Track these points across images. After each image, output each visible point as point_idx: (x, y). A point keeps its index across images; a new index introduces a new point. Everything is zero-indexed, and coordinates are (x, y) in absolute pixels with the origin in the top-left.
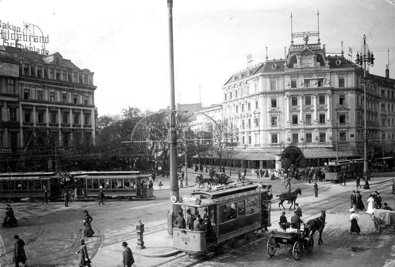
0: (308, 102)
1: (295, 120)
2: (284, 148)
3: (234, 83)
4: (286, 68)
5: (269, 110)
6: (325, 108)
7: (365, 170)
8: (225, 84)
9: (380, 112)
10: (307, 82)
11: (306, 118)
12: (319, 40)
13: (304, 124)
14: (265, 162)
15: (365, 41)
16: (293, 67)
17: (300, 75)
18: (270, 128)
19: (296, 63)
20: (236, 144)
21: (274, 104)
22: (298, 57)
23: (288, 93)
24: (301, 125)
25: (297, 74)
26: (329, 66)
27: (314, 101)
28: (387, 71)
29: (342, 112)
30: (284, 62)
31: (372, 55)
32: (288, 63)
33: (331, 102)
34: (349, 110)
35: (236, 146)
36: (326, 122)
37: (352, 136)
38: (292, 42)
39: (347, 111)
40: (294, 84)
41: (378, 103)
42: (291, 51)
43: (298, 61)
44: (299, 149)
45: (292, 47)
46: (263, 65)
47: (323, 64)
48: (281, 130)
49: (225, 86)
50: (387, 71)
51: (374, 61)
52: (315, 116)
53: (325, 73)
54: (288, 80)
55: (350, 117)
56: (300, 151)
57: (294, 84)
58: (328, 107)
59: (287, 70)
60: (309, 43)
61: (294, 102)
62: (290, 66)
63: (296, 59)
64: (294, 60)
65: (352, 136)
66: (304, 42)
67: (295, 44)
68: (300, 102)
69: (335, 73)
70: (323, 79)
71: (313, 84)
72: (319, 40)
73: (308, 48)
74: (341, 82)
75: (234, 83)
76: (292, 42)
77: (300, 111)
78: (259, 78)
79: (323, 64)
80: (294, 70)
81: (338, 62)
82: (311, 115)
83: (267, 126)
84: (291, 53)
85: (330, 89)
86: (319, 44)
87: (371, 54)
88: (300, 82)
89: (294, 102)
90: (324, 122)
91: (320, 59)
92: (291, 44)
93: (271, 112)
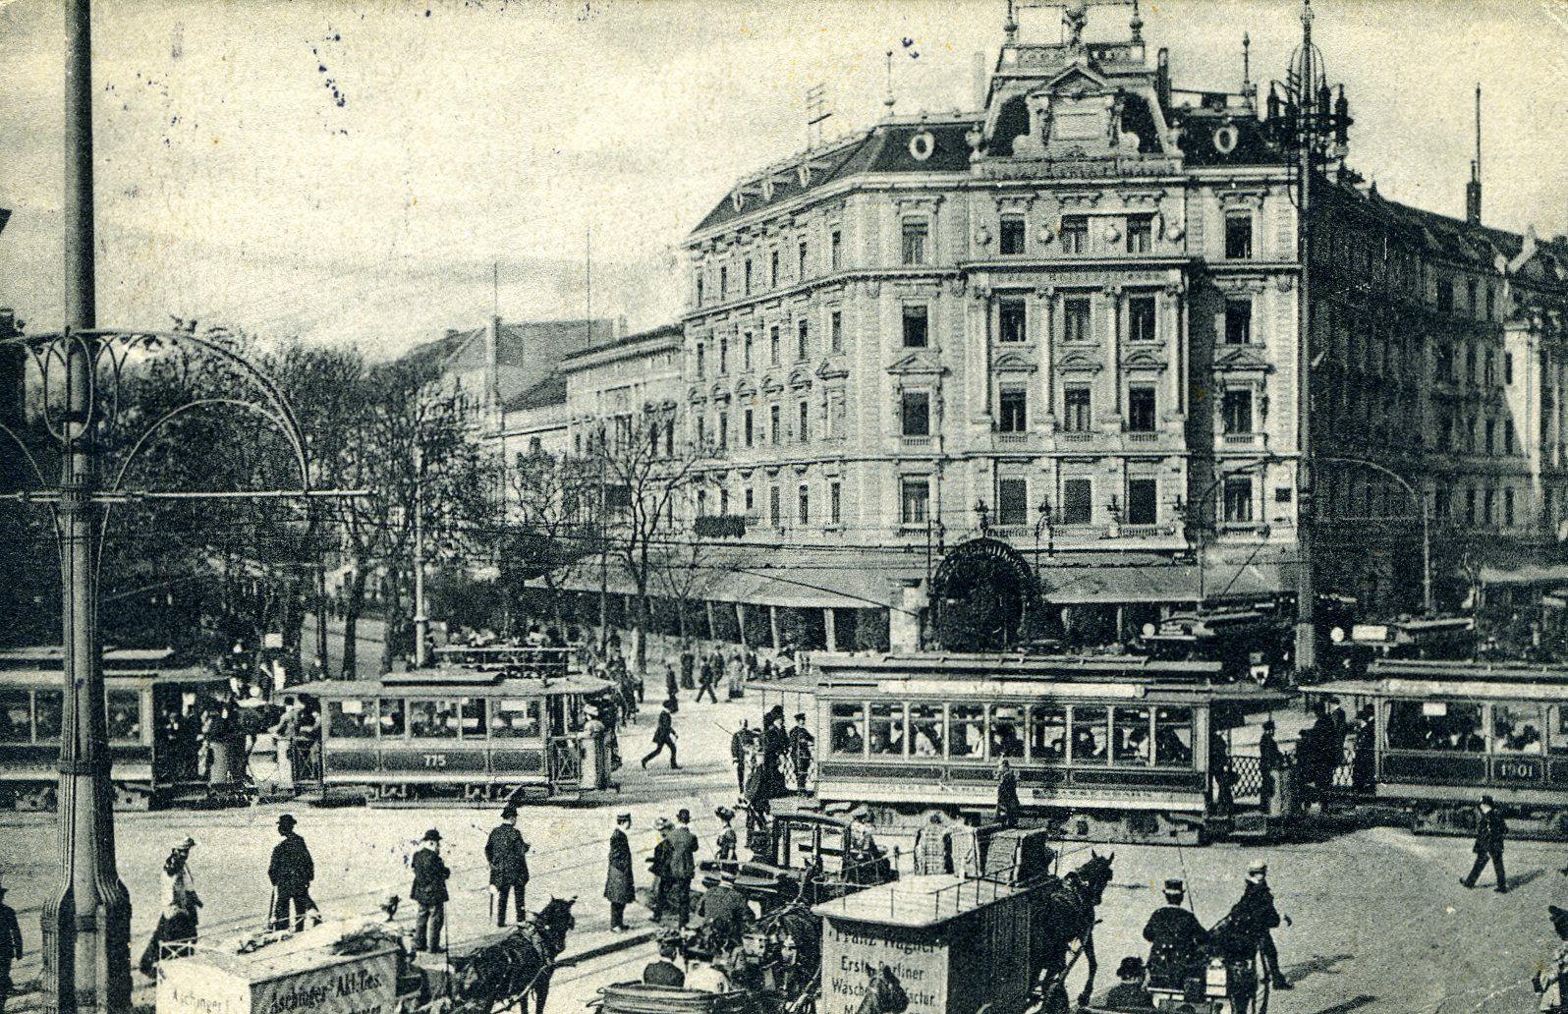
0: (1143, 322)
1: (1011, 412)
2: (941, 549)
3: (741, 222)
4: (976, 155)
5: (887, 357)
6: (1098, 358)
7: (170, 785)
8: (701, 227)
9: (1427, 384)
10: (1075, 226)
11: (1069, 402)
12: (1137, 26)
13: (1123, 430)
14: (845, 617)
15: (1307, 28)
16: (1010, 152)
17: (1045, 194)
18: (895, 446)
19: (1027, 132)
20: (738, 525)
21: (915, 329)
22: (1032, 105)
23: (983, 280)
24: (1040, 433)
25: (1031, 189)
26: (1180, 153)
27: (1106, 323)
28: (1474, 190)
29: (917, 385)
30: (968, 127)
31: (1342, 103)
32: (989, 131)
33: (1305, 321)
34: (1269, 370)
35: (741, 533)
36: (1028, 428)
37: (1283, 495)
38: (1012, 29)
39: (1260, 375)
40: (1011, 235)
41: (1420, 340)
42: (1005, 73)
43: (1035, 122)
44: (1016, 555)
45: (1011, 56)
46: (870, 136)
47: (1150, 144)
48: (949, 460)
49: (700, 236)
50: (1474, 190)
51: (1350, 130)
52: (1107, 397)
53: (1160, 186)
54: (985, 213)
55: (1273, 406)
56: (1025, 566)
57: (1011, 235)
58: (1171, 355)
59: (980, 166)
60: (1087, 36)
61: (1012, 322)
62: (1000, 146)
63: (1027, 115)
64: (1014, 118)
65: (1283, 495)
66: (1067, 35)
67: (1023, 38)
68: (1038, 318)
69: (1206, 190)
70: (1148, 217)
71: (1103, 236)
72: (1137, 26)
73: (1083, 60)
74: (1238, 236)
75: (741, 222)
76: (1012, 29)
77: (1165, 367)
78: (949, 196)
79: (1150, 144)
80: (1012, 169)
81: (1225, 137)
82: (1087, 392)
83: (879, 436)
84: (999, 82)
85: (1183, 268)
86: (1138, 41)
87: (1334, 98)
88: (1042, 218)
89: (1012, 322)
90: (1022, 426)
91: (1133, 114)
92: (1003, 38)
93: (897, 369)
